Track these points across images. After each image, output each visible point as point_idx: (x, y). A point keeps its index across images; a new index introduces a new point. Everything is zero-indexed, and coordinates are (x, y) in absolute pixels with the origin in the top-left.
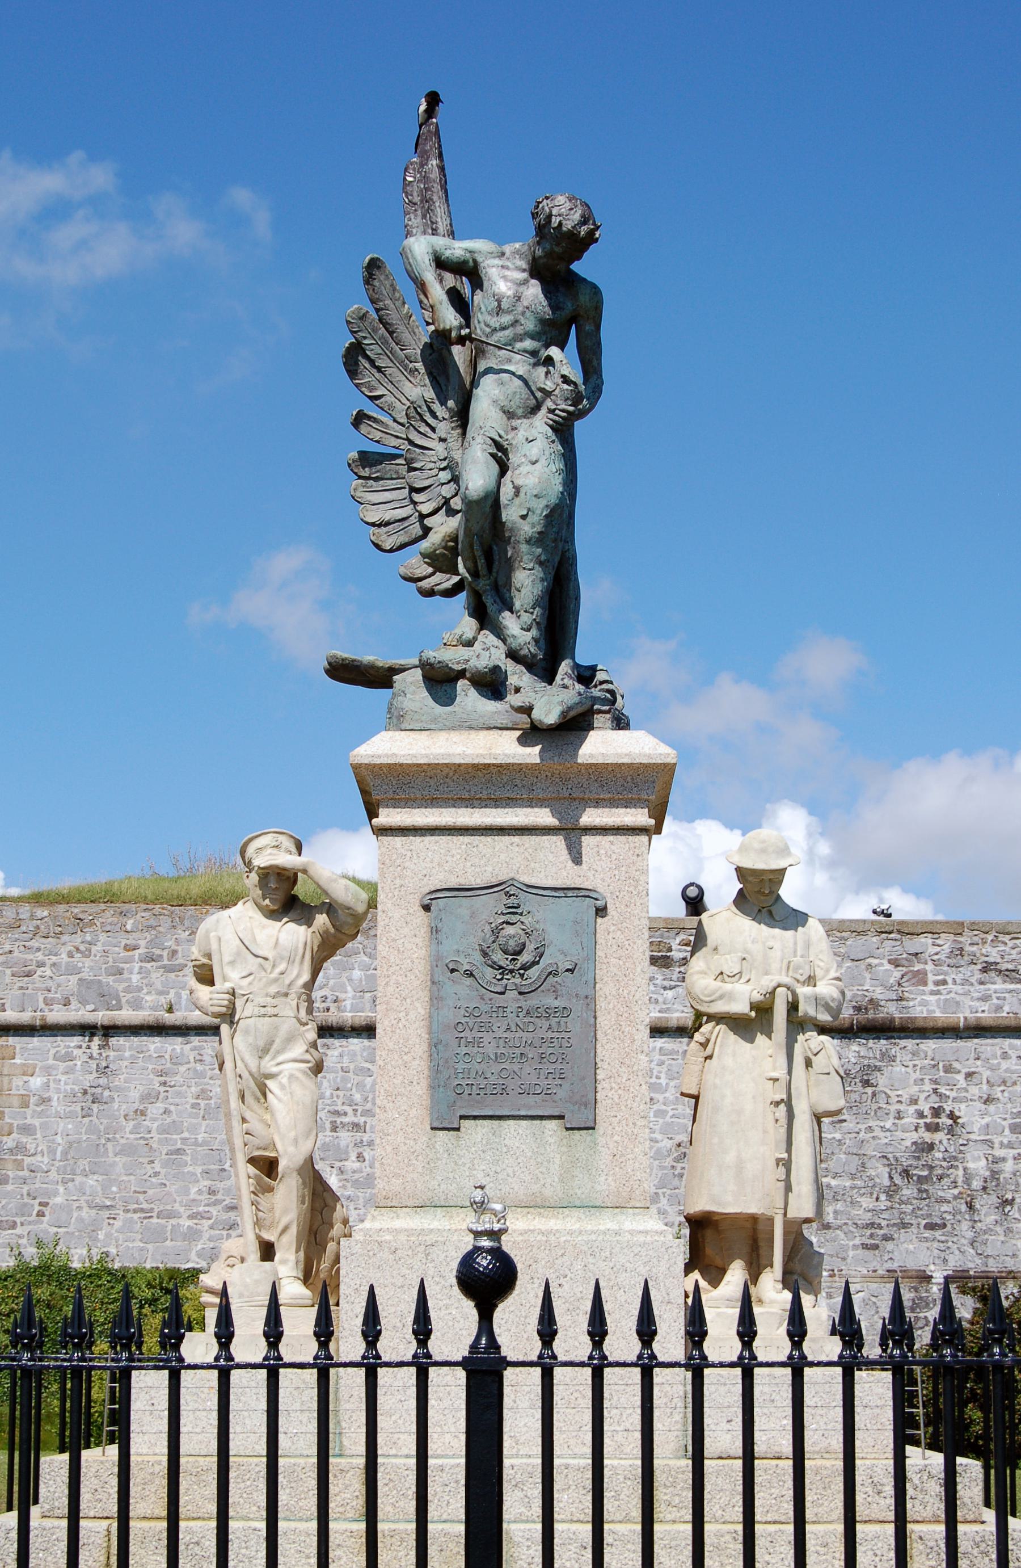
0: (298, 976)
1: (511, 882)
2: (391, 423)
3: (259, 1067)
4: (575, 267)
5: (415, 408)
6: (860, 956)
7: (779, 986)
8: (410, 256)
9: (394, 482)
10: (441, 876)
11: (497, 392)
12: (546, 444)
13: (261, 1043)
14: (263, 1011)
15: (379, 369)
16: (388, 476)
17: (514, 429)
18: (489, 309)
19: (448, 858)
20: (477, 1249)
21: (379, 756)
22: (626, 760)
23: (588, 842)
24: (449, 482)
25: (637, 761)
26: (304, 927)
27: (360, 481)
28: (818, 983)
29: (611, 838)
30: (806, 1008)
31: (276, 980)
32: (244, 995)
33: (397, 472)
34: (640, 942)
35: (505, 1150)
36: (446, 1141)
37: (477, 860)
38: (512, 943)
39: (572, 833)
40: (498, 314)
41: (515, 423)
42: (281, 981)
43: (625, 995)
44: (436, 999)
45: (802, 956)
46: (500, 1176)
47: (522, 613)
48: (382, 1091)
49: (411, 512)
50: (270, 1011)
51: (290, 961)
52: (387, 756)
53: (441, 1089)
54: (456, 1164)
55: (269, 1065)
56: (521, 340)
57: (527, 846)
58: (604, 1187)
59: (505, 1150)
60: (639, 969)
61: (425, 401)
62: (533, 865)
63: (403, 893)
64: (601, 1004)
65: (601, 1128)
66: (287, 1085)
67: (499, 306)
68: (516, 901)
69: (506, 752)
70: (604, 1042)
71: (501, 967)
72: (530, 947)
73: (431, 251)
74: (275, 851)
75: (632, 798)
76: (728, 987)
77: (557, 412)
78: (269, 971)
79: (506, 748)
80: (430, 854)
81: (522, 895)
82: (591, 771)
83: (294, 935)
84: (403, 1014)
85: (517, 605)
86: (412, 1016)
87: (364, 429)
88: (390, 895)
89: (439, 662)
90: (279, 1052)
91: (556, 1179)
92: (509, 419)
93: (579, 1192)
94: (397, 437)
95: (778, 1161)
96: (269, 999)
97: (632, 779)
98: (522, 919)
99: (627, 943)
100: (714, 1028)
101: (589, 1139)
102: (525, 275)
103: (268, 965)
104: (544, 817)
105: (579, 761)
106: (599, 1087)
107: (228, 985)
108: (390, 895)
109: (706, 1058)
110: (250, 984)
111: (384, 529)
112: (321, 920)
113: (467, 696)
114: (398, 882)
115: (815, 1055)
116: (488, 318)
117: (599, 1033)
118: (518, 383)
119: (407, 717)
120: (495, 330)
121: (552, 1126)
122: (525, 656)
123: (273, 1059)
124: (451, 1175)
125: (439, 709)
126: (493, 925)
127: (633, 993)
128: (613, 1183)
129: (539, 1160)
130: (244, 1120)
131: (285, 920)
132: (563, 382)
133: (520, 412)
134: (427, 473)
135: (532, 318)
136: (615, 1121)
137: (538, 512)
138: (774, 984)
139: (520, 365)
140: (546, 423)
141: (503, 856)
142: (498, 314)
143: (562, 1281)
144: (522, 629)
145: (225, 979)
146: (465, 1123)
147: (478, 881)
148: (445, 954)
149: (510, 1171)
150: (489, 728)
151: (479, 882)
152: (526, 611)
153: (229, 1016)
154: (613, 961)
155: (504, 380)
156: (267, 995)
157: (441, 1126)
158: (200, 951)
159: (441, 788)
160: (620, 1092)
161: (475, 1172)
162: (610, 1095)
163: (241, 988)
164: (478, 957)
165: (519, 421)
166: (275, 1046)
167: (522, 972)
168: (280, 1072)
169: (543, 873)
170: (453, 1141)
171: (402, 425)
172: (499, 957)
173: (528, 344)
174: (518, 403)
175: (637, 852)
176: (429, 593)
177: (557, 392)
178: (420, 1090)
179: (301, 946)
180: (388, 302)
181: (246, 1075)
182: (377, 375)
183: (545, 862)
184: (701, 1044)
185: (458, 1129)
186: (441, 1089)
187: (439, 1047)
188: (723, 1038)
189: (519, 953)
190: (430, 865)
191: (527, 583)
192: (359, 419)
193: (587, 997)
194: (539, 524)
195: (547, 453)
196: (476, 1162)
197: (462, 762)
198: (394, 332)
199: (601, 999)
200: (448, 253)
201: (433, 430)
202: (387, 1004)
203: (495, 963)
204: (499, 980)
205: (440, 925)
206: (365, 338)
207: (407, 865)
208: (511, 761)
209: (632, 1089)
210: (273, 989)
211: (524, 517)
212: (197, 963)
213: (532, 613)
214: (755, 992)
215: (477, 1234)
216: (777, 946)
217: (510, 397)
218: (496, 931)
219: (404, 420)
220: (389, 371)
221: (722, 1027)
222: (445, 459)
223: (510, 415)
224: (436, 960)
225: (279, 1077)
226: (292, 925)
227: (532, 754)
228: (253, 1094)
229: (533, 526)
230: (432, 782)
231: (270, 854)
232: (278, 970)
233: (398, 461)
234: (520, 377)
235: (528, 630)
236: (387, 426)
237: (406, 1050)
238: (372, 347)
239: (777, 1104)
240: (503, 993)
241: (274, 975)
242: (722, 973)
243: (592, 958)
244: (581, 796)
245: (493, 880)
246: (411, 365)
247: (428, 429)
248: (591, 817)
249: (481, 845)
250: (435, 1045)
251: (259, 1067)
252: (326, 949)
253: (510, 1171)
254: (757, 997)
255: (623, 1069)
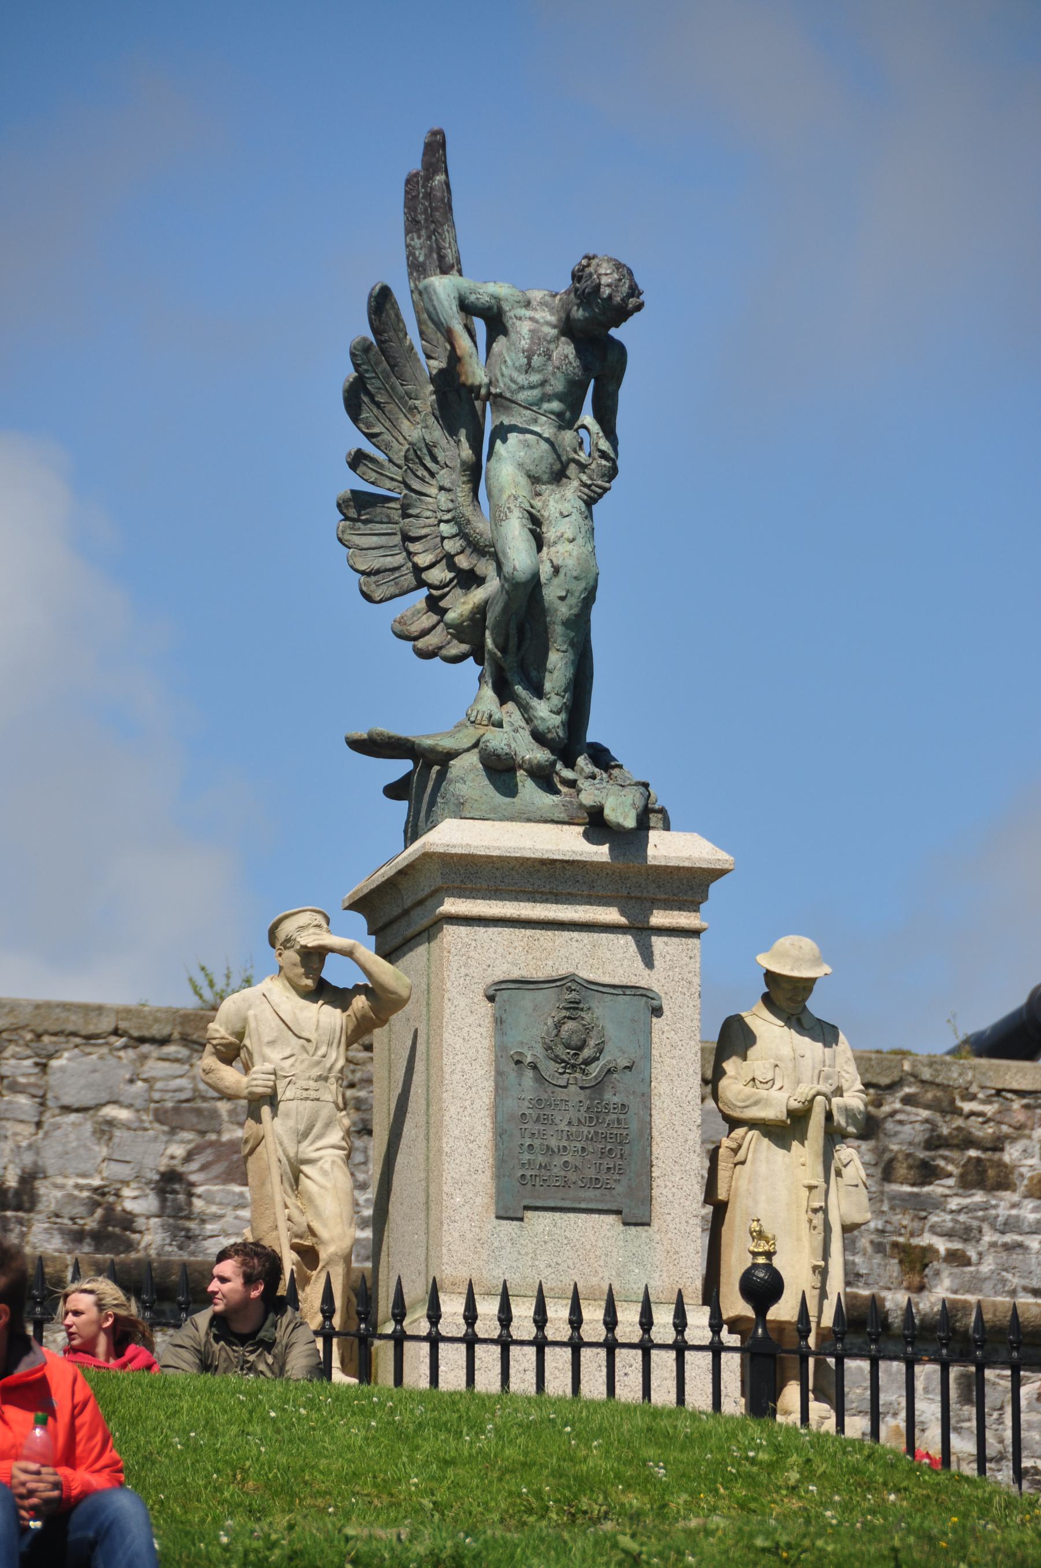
0: (336, 1060)
1: (572, 978)
2: (386, 463)
3: (297, 1152)
4: (613, 332)
5: (415, 451)
6: (87, 1098)
7: (818, 1094)
8: (434, 298)
9: (384, 526)
10: (505, 967)
11: (522, 454)
12: (580, 520)
13: (302, 1128)
14: (305, 1094)
15: (378, 405)
16: (378, 519)
17: (538, 494)
18: (517, 364)
19: (511, 950)
20: (755, 1266)
21: (454, 846)
22: (687, 864)
23: (658, 943)
24: (454, 536)
25: (697, 865)
26: (339, 1011)
27: (348, 523)
28: (845, 1094)
29: (665, 939)
30: (839, 1119)
31: (318, 1063)
32: (286, 1077)
33: (388, 516)
34: (693, 1043)
35: (566, 1242)
36: (510, 1230)
37: (538, 954)
38: (575, 1038)
39: (641, 932)
40: (526, 372)
41: (540, 488)
42: (322, 1064)
43: (678, 1094)
44: (500, 1089)
45: (830, 1066)
46: (561, 1268)
47: (553, 695)
48: (449, 1178)
49: (402, 561)
50: (313, 1094)
51: (330, 1044)
52: (462, 846)
53: (506, 1178)
54: (519, 1253)
55: (307, 1150)
56: (549, 401)
57: (586, 942)
58: (659, 1283)
59: (566, 1242)
60: (691, 1071)
61: (427, 445)
62: (591, 961)
63: (468, 982)
64: (656, 1102)
65: (655, 1223)
66: (329, 1170)
67: (529, 364)
68: (578, 997)
69: (574, 849)
70: (659, 1140)
71: (563, 1061)
72: (592, 1043)
73: (457, 295)
74: (317, 930)
75: (686, 901)
76: (763, 1093)
77: (593, 487)
78: (311, 1053)
79: (569, 843)
80: (493, 944)
81: (584, 992)
82: (650, 872)
83: (328, 1018)
84: (468, 1103)
85: (548, 686)
86: (478, 1104)
87: (361, 469)
88: (456, 983)
89: (507, 754)
90: (320, 1137)
91: (614, 1273)
92: (533, 484)
93: (635, 1287)
94: (392, 479)
95: (815, 1268)
96: (312, 1083)
97: (688, 882)
98: (583, 1014)
99: (680, 1043)
100: (746, 1133)
101: (644, 1235)
102: (554, 332)
103: (311, 1048)
104: (611, 915)
105: (651, 861)
106: (654, 1184)
107: (268, 1067)
108: (456, 983)
109: (736, 1165)
110: (292, 1065)
111: (373, 578)
112: (360, 1002)
113: (528, 789)
114: (463, 971)
115: (845, 1166)
116: (515, 375)
117: (654, 1130)
118: (545, 446)
119: (467, 805)
120: (522, 388)
121: (611, 1219)
122: (553, 739)
123: (313, 1142)
124: (514, 1264)
125: (500, 799)
126: (556, 1019)
127: (686, 1093)
128: (666, 1279)
129: (597, 1253)
130: (286, 1207)
131: (321, 1002)
132: (600, 457)
133: (545, 477)
134: (422, 522)
135: (562, 379)
136: (669, 1218)
137: (577, 594)
138: (813, 1092)
139: (546, 428)
140: (579, 497)
141: (562, 951)
142: (526, 372)
143: (628, 1370)
144: (551, 711)
145: (265, 1059)
146: (529, 1214)
147: (540, 974)
148: (509, 1045)
149: (570, 1262)
150: (546, 821)
151: (540, 975)
152: (557, 694)
153: (272, 1099)
154: (667, 1061)
155: (531, 442)
156: (309, 1078)
157: (505, 1215)
158: (227, 1029)
159: (506, 880)
160: (674, 1190)
161: (537, 1263)
162: (664, 1192)
163: (282, 1069)
164: (539, 1051)
165: (544, 487)
166: (315, 1131)
167: (583, 1066)
168: (321, 1158)
169: (601, 970)
170: (516, 1231)
171: (399, 467)
172: (561, 1051)
173: (555, 405)
174: (544, 469)
175: (690, 954)
176: (426, 655)
177: (593, 466)
178: (485, 1179)
179: (338, 1029)
180: (392, 333)
181: (284, 1160)
182: (375, 410)
183: (612, 960)
184: (732, 1149)
185: (521, 1219)
186: (506, 1178)
187: (504, 1136)
188: (756, 1144)
189: (580, 1048)
190: (494, 956)
191: (558, 664)
192: (357, 460)
193: (643, 1095)
194: (577, 606)
195: (583, 530)
196: (538, 1252)
197: (533, 856)
198: (396, 365)
199: (656, 1098)
200: (473, 298)
201: (432, 475)
202: (453, 1092)
203: (557, 1056)
204: (561, 1074)
205: (504, 1016)
206: (367, 371)
207: (472, 954)
208: (579, 858)
209: (685, 1188)
210: (316, 1072)
211: (562, 599)
212: (224, 1041)
213: (563, 697)
214: (792, 1099)
215: (755, 1254)
216: (808, 1055)
217: (536, 462)
218: (558, 1025)
219: (401, 462)
220: (388, 407)
221: (754, 1133)
222: (449, 511)
223: (534, 480)
224: (500, 1050)
225: (320, 1163)
226: (327, 1008)
227: (601, 853)
228: (289, 1181)
229: (571, 608)
230: (498, 873)
231: (314, 934)
232: (320, 1052)
233: (392, 505)
234: (547, 440)
235: (558, 713)
236: (382, 466)
237: (472, 1138)
238: (373, 381)
239: (815, 1211)
240: (565, 1087)
241: (316, 1058)
242: (753, 1080)
243: (648, 1056)
244: (639, 894)
245: (554, 974)
246: (411, 402)
247: (426, 474)
248: (659, 918)
249: (542, 939)
250: (500, 1134)
251: (297, 1152)
252: (359, 1034)
253: (570, 1262)
254: (794, 1105)
255: (677, 1168)
